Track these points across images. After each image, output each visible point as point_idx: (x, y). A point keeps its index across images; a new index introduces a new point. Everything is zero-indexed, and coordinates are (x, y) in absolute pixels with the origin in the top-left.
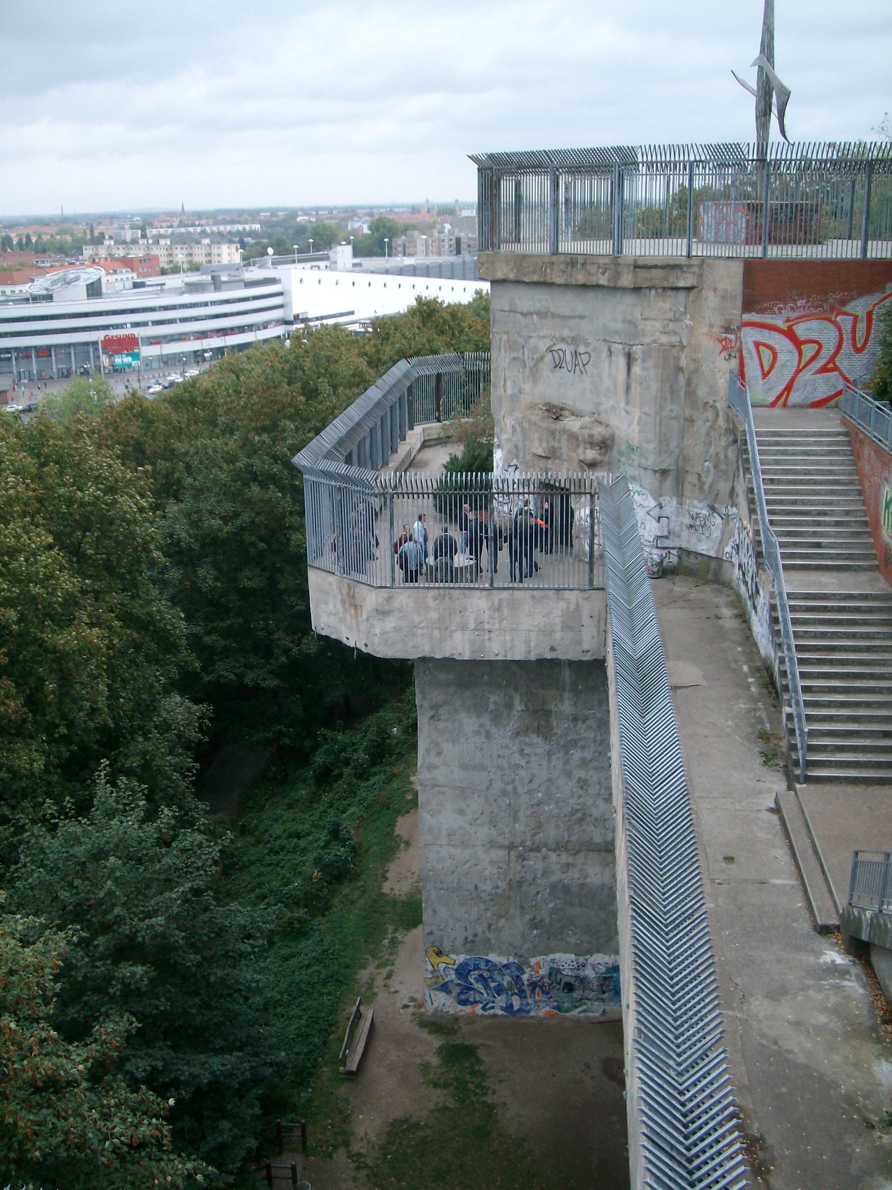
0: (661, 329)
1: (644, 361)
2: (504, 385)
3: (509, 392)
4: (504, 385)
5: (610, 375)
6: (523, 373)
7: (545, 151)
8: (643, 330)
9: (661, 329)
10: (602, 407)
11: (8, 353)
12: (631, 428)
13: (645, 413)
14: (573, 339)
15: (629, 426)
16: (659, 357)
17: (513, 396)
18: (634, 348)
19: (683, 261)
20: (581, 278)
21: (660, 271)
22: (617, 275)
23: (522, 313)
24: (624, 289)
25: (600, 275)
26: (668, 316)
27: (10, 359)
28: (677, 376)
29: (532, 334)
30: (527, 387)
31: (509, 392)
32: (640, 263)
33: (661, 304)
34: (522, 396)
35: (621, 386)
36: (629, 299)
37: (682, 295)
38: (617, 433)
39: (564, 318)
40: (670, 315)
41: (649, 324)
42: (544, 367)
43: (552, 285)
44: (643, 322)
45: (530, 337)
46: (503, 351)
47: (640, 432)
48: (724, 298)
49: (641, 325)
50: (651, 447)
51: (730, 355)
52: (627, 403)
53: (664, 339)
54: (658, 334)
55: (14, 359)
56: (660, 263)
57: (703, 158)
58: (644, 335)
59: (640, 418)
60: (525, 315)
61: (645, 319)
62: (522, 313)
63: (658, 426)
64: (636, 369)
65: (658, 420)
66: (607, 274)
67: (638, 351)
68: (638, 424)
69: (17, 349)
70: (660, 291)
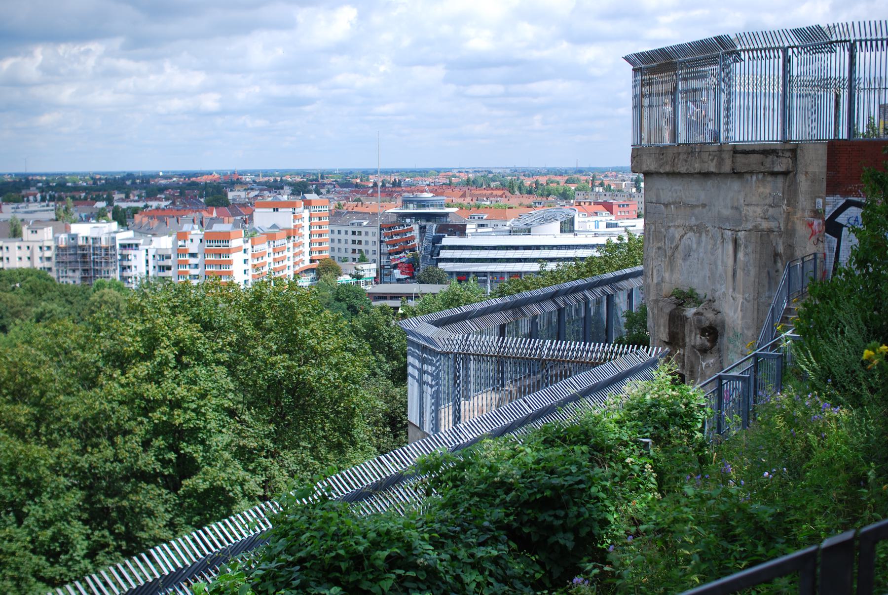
0: (762, 215)
1: (746, 247)
2: (652, 274)
3: (655, 281)
4: (652, 274)
5: (722, 262)
6: (665, 262)
7: (689, 44)
8: (746, 216)
9: (762, 215)
10: (717, 294)
11: (485, 276)
12: (736, 315)
13: (746, 299)
14: (698, 226)
15: (735, 313)
16: (756, 242)
17: (658, 284)
18: (739, 233)
19: (779, 146)
20: (697, 167)
21: (757, 156)
22: (721, 161)
23: (664, 204)
24: (726, 175)
25: (710, 162)
26: (767, 201)
27: (485, 282)
28: (775, 262)
29: (671, 224)
30: (667, 275)
31: (655, 281)
32: (739, 149)
33: (761, 190)
34: (663, 284)
35: (730, 273)
36: (735, 185)
37: (780, 180)
38: (726, 318)
39: (693, 207)
40: (769, 201)
41: (751, 209)
42: (679, 256)
43: (679, 174)
44: (746, 208)
45: (669, 227)
46: (651, 241)
47: (743, 318)
48: (813, 181)
49: (745, 210)
50: (749, 333)
51: (818, 240)
52: (734, 289)
53: (765, 225)
54: (759, 219)
55: (489, 281)
56: (757, 149)
57: (797, 44)
58: (747, 221)
59: (743, 303)
60: (666, 205)
61: (748, 205)
62: (664, 204)
63: (756, 313)
64: (741, 255)
65: (756, 307)
66: (715, 161)
67: (742, 237)
68: (741, 310)
69: (492, 273)
70: (760, 176)
